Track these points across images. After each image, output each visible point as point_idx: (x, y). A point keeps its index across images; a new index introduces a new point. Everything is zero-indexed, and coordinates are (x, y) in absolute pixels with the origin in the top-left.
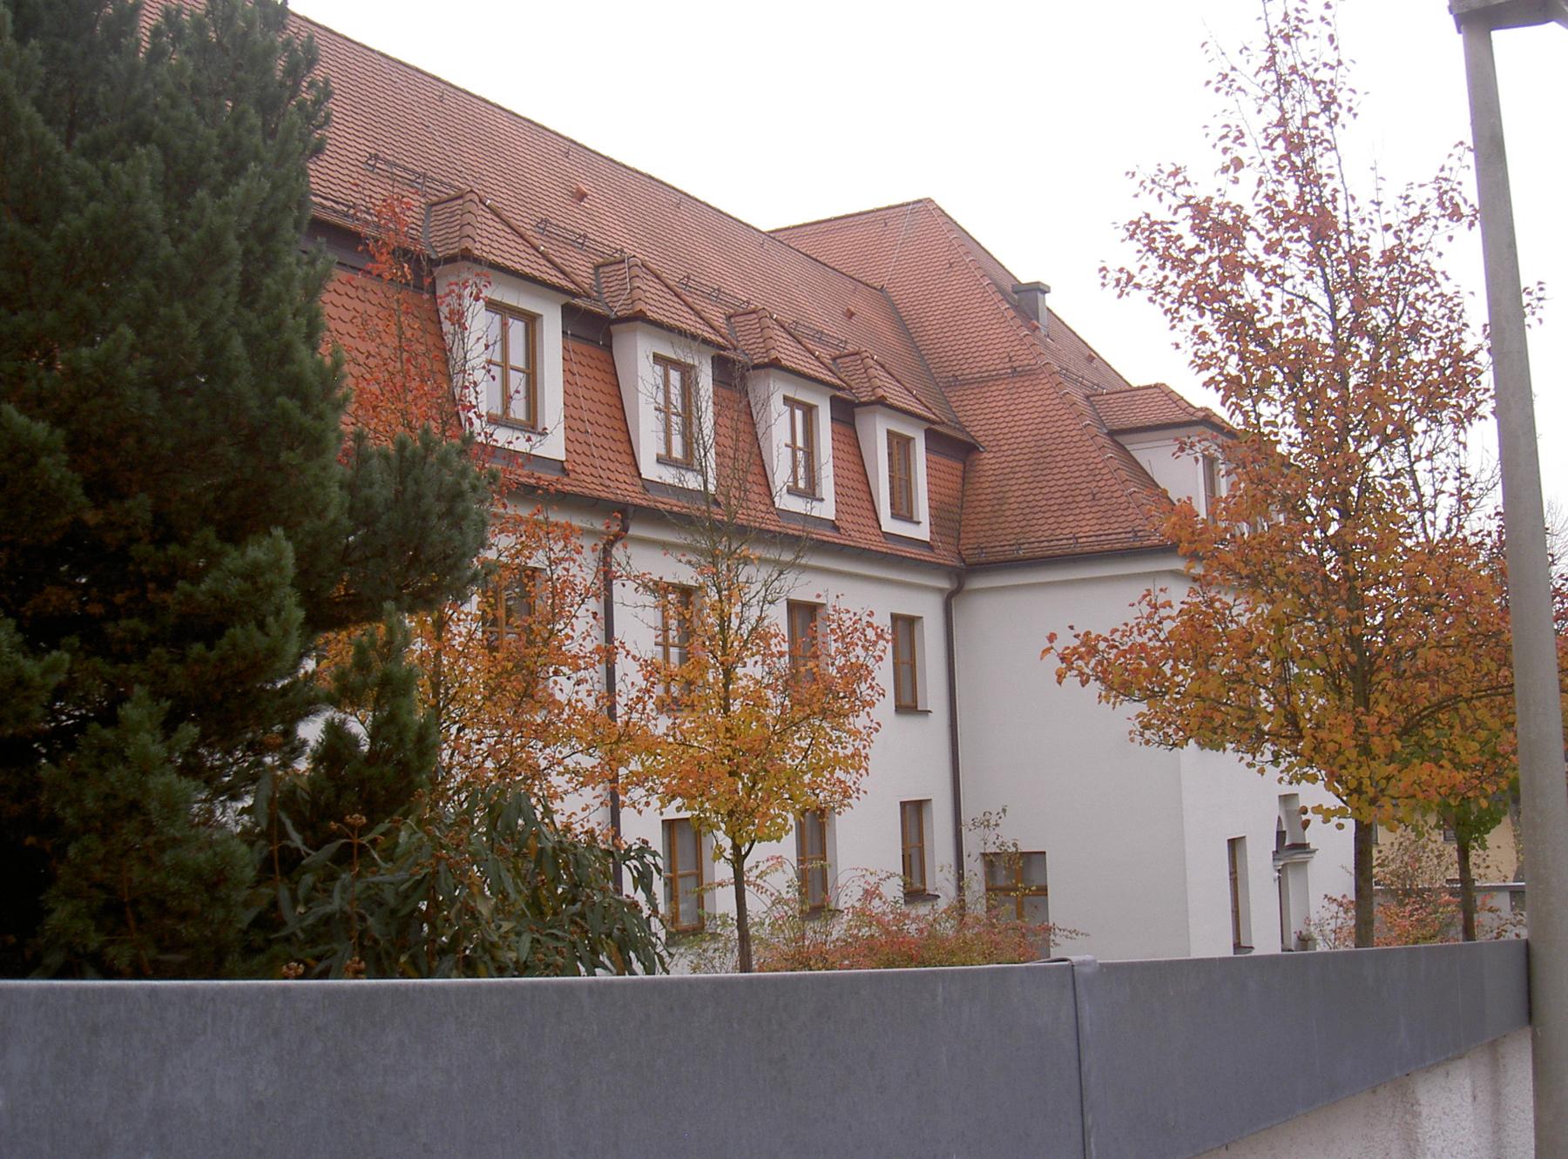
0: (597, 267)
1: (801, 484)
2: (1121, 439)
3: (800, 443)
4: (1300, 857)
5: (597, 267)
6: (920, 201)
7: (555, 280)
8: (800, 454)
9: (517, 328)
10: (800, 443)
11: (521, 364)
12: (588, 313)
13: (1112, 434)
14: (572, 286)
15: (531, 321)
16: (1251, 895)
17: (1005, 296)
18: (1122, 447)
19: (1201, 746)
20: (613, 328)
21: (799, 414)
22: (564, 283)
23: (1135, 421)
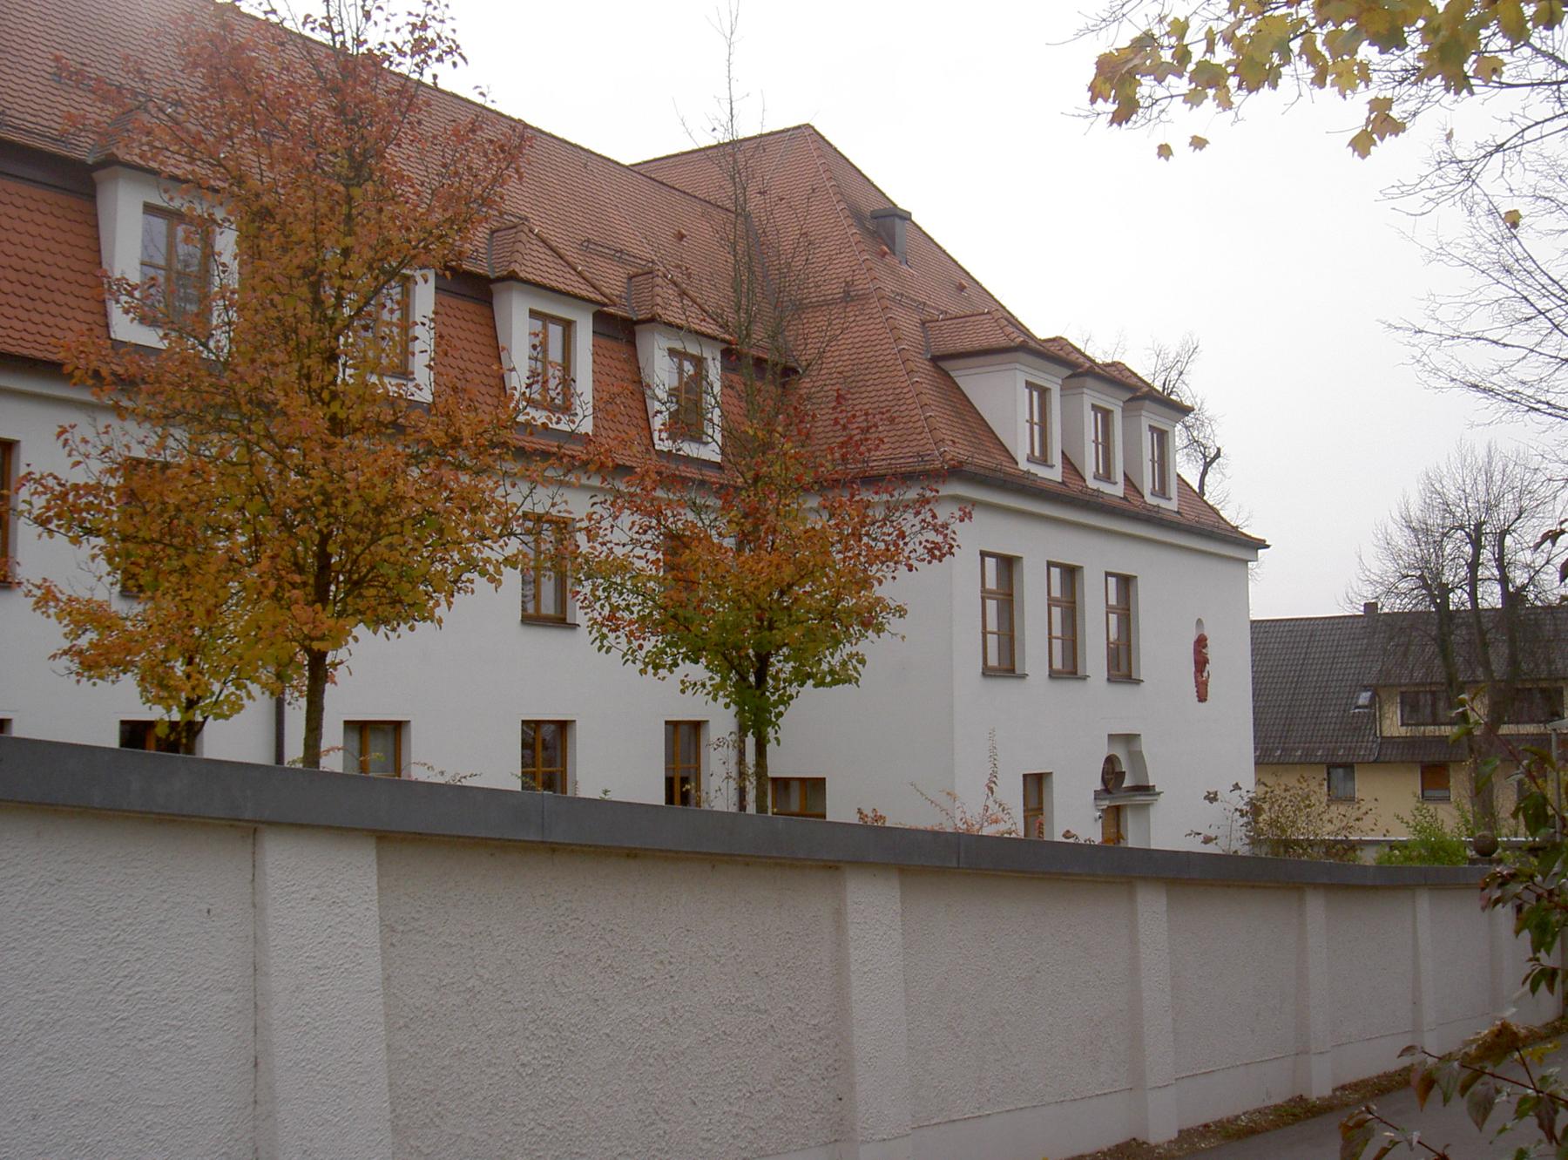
0: (630, 278)
1: (1037, 453)
2: (945, 365)
3: (1036, 419)
4: (1140, 799)
5: (630, 278)
6: (799, 127)
7: (584, 293)
8: (1036, 428)
9: (555, 332)
10: (1036, 419)
11: (559, 359)
12: (611, 315)
13: (935, 360)
14: (599, 298)
15: (568, 325)
16: (1055, 801)
17: (857, 216)
18: (946, 375)
19: (376, 622)
20: (637, 328)
21: (1035, 394)
22: (592, 296)
23: (967, 345)
